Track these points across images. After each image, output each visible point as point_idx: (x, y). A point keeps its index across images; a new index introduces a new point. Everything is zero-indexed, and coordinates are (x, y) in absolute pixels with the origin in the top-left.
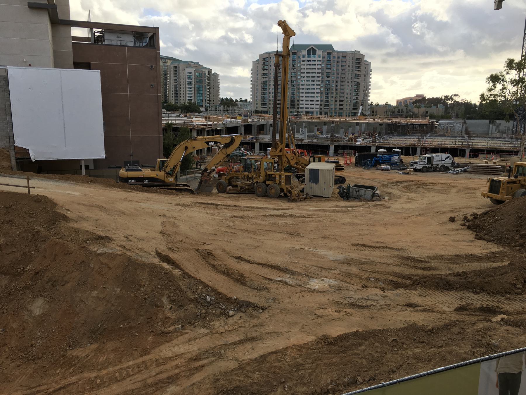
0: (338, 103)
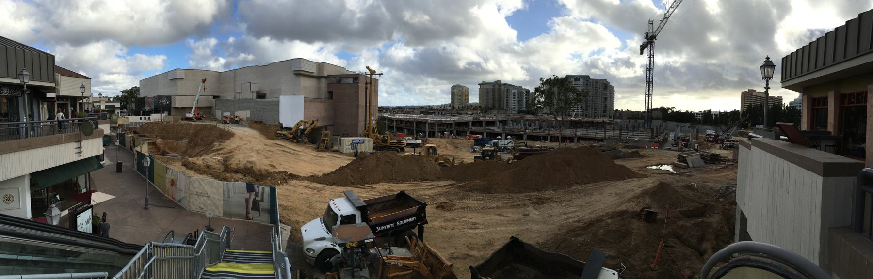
0: (593, 109)
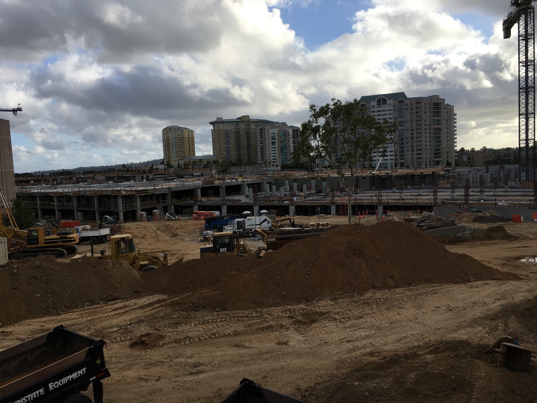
0: (415, 153)
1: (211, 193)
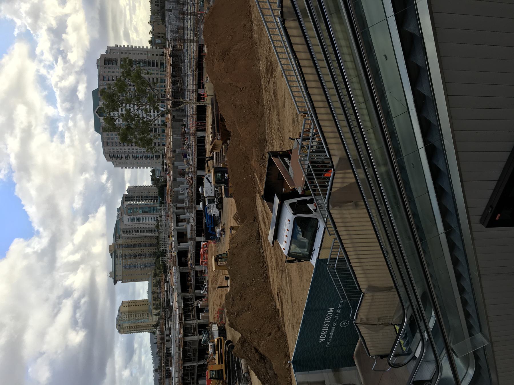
1: (184, 259)
